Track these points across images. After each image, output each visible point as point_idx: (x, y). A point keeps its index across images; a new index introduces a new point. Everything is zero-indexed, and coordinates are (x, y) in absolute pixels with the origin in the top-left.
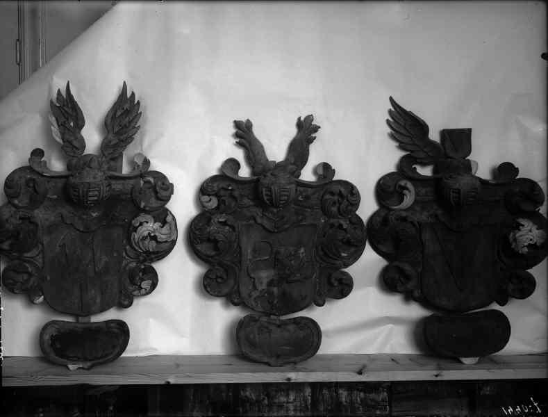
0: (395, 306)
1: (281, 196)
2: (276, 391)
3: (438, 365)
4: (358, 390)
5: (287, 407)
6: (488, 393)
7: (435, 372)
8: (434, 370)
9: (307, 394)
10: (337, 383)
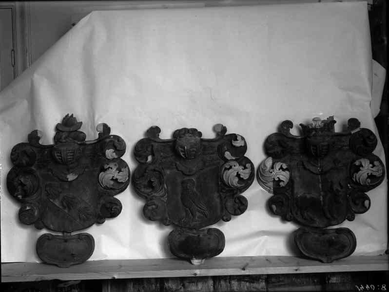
0: (276, 224)
1: (67, 159)
4: (245, 281)
6: (335, 282)
7: (295, 268)
10: (230, 276)
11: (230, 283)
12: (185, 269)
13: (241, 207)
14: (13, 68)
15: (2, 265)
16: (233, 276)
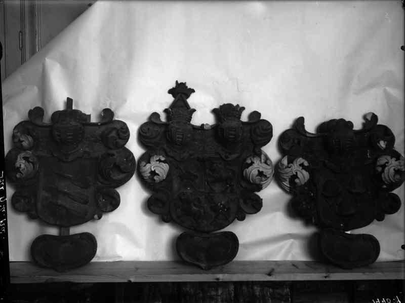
0: (297, 228)
11: (252, 288)
13: (256, 206)
15: (10, 264)
16: (256, 282)
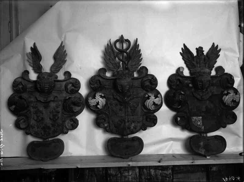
2: (124, 170)
3: (193, 158)
4: (158, 169)
5: (128, 177)
6: (215, 170)
7: (191, 161)
8: (191, 160)
9: (137, 171)
10: (150, 166)
11: (149, 171)
12: (123, 161)
13: (153, 121)
14: (9, 33)
16: (151, 166)
